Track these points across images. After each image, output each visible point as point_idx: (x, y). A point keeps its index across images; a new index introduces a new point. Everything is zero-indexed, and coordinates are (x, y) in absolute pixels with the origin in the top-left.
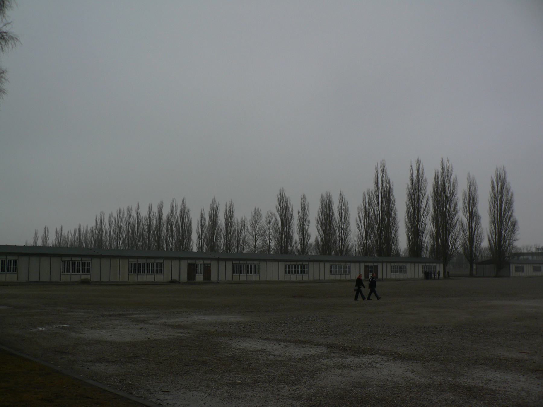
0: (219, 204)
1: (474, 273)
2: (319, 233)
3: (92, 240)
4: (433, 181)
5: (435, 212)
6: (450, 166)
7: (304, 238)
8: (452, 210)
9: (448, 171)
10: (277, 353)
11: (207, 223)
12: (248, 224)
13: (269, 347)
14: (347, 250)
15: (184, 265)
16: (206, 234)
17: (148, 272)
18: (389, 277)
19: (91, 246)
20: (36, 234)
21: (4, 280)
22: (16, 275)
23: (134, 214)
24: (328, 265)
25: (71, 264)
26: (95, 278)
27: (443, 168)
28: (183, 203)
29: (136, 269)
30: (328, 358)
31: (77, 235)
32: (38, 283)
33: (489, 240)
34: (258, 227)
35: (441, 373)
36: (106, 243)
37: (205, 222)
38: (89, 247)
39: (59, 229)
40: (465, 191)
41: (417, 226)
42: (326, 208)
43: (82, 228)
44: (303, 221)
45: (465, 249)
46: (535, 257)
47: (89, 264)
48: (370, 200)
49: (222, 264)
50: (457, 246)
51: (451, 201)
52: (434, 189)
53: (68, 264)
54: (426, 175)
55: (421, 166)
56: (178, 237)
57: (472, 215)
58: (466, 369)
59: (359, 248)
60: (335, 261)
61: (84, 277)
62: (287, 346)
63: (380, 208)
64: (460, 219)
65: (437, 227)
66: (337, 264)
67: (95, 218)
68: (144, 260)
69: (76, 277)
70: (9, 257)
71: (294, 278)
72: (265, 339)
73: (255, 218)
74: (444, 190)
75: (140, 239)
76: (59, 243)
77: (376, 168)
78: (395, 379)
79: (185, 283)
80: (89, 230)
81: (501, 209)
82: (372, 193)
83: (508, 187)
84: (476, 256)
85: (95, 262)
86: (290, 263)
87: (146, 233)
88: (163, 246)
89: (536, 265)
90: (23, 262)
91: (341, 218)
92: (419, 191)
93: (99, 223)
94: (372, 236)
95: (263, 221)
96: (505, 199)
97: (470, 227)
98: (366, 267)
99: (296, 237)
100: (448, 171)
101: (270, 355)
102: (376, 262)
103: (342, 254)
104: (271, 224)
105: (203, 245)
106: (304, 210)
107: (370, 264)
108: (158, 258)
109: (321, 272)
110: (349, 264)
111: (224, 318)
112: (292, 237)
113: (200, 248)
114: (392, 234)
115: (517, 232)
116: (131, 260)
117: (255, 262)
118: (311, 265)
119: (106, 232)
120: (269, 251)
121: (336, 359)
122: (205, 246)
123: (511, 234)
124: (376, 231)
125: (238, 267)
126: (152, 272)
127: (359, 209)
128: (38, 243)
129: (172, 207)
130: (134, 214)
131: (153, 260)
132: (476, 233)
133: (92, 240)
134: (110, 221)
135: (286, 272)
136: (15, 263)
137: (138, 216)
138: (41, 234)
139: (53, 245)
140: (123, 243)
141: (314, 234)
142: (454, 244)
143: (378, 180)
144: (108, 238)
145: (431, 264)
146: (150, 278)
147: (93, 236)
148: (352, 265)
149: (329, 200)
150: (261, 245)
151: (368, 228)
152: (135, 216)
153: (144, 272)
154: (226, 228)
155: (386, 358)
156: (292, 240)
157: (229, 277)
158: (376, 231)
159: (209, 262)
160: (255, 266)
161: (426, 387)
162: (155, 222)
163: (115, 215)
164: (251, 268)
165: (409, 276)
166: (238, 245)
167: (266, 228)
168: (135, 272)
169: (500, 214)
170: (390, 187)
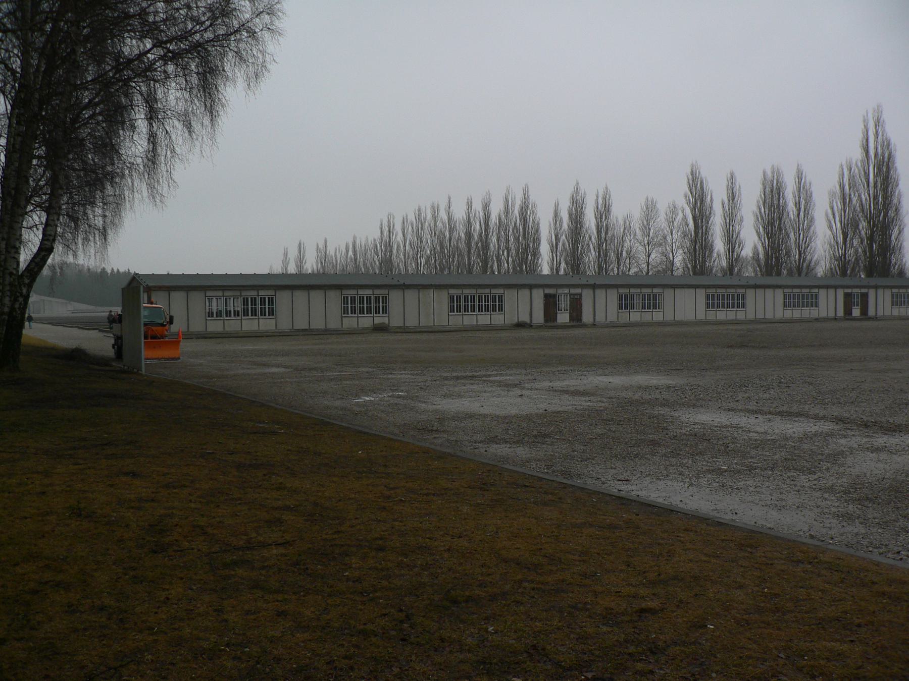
0: (585, 194)
2: (760, 238)
7: (733, 248)
10: (758, 429)
11: (565, 226)
12: (636, 226)
14: (809, 266)
15: (538, 297)
16: (564, 244)
17: (480, 310)
18: (887, 313)
19: (374, 269)
21: (255, 328)
22: (274, 321)
23: (443, 215)
24: (779, 293)
26: (396, 322)
28: (525, 194)
29: (455, 305)
31: (351, 253)
32: (308, 333)
37: (561, 226)
38: (371, 272)
39: (321, 246)
42: (773, 195)
43: (358, 242)
47: (385, 300)
48: (852, 178)
49: (600, 293)
61: (378, 320)
63: (871, 192)
66: (795, 290)
67: (379, 224)
68: (474, 291)
69: (366, 321)
70: (262, 293)
71: (721, 315)
73: (647, 215)
75: (454, 257)
76: (323, 267)
77: (864, 121)
79: (540, 327)
82: (857, 166)
85: (395, 298)
87: (462, 245)
88: (492, 266)
90: (283, 299)
91: (799, 210)
93: (386, 233)
95: (661, 221)
98: (847, 295)
99: (719, 246)
103: (800, 275)
104: (675, 224)
106: (733, 199)
107: (855, 290)
109: (767, 306)
110: (816, 290)
112: (712, 246)
114: (893, 238)
116: (452, 291)
117: (655, 290)
118: (750, 293)
119: (398, 246)
120: (672, 271)
121: (859, 438)
122: (563, 265)
124: (863, 233)
125: (487, 300)
127: (832, 194)
130: (443, 215)
131: (487, 291)
135: (708, 306)
136: (271, 301)
137: (450, 219)
138: (293, 254)
140: (426, 263)
141: (751, 241)
143: (867, 140)
144: (402, 256)
146: (484, 319)
148: (822, 293)
149: (778, 181)
151: (849, 227)
152: (445, 218)
154: (599, 232)
156: (711, 251)
157: (612, 317)
158: (863, 233)
159: (578, 291)
162: (478, 227)
163: (412, 217)
164: (649, 299)
166: (618, 262)
167: (667, 231)
168: (459, 310)
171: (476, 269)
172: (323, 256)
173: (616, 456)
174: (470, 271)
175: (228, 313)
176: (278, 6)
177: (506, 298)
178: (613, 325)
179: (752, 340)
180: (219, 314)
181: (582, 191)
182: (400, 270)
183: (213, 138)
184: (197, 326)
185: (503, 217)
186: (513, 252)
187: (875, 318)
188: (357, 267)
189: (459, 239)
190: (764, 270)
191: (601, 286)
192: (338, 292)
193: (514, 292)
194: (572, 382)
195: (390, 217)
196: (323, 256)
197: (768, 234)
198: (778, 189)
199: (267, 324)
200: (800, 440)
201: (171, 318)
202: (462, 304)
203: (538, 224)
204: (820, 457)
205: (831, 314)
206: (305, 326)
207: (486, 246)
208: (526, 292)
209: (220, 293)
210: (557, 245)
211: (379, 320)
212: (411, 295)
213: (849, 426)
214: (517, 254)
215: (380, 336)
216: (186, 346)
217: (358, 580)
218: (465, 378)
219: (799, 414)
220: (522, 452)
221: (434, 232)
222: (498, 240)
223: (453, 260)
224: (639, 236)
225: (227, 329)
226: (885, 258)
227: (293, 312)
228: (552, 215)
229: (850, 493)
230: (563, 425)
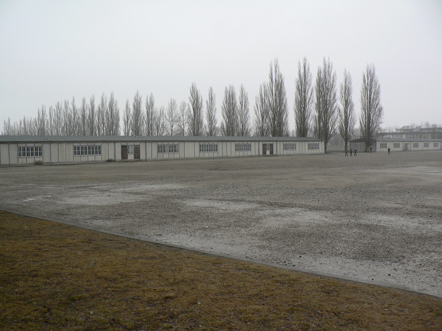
3: (36, 129)
5: (318, 100)
6: (331, 63)
7: (212, 123)
8: (332, 99)
9: (329, 67)
10: (223, 208)
11: (132, 112)
12: (166, 112)
13: (216, 204)
14: (247, 131)
15: (118, 147)
16: (131, 121)
17: (89, 153)
18: (282, 153)
19: (35, 134)
23: (70, 106)
24: (233, 144)
25: (26, 149)
27: (325, 65)
28: (111, 96)
30: (262, 210)
31: (22, 125)
33: (361, 123)
36: (48, 131)
37: (129, 112)
38: (33, 135)
41: (304, 111)
42: (230, 99)
44: (211, 109)
45: (341, 130)
46: (395, 136)
48: (265, 91)
49: (149, 145)
50: (335, 127)
52: (317, 81)
56: (108, 124)
57: (347, 103)
58: (363, 214)
60: (286, 141)
62: (228, 204)
63: (274, 98)
64: (338, 106)
65: (319, 112)
67: (38, 110)
68: (86, 144)
69: (31, 160)
71: (207, 155)
72: (209, 199)
73: (171, 107)
74: (326, 83)
75: (76, 127)
76: (8, 132)
81: (370, 98)
83: (376, 80)
84: (350, 136)
85: (46, 148)
87: (81, 121)
88: (95, 132)
89: (396, 142)
91: (242, 105)
92: (306, 83)
93: (41, 115)
94: (267, 120)
95: (178, 110)
96: (373, 90)
97: (346, 112)
98: (264, 145)
99: (205, 122)
100: (329, 67)
101: (219, 209)
102: (272, 141)
103: (243, 136)
104: (185, 111)
105: (129, 130)
106: (212, 100)
107: (267, 143)
109: (228, 150)
110: (250, 143)
111: (168, 186)
112: (202, 122)
113: (127, 133)
115: (382, 117)
116: (75, 144)
117: (175, 143)
118: (220, 144)
119: (48, 122)
120: (183, 134)
122: (131, 131)
123: (377, 118)
124: (270, 116)
127: (257, 98)
129: (103, 99)
130: (70, 106)
131: (93, 144)
133: (36, 129)
135: (200, 151)
137: (74, 108)
140: (62, 130)
141: (220, 120)
142: (333, 126)
143: (272, 74)
144: (49, 127)
145: (315, 143)
146: (91, 158)
147: (36, 125)
150: (177, 129)
151: (264, 114)
155: (303, 209)
156: (202, 125)
157: (155, 156)
158: (270, 116)
159: (138, 144)
160: (175, 146)
162: (88, 112)
163: (54, 107)
164: (172, 147)
165: (298, 152)
167: (181, 115)
168: (78, 154)
169: (370, 102)
170: (282, 81)
171: (88, 133)
173: (155, 224)
174: (84, 135)
177: (102, 148)
178: (155, 160)
179: (220, 166)
181: (140, 95)
182: (48, 134)
185: (101, 107)
186: (106, 125)
187: (276, 155)
188: (26, 132)
189: (79, 118)
190: (226, 133)
191: (149, 141)
192: (16, 145)
194: (134, 188)
195: (43, 106)
197: (228, 116)
198: (232, 95)
200: (242, 212)
204: (251, 220)
205: (257, 154)
206: (7, 163)
207: (92, 122)
208: (112, 144)
210: (127, 121)
211: (38, 159)
212: (54, 146)
213: (264, 205)
214: (108, 126)
215: (39, 167)
217: (23, 293)
219: (242, 201)
220: (109, 223)
221: (66, 114)
222: (98, 119)
223: (76, 129)
224: (167, 117)
226: (280, 128)
228: (125, 106)
229: (264, 236)
230: (130, 209)
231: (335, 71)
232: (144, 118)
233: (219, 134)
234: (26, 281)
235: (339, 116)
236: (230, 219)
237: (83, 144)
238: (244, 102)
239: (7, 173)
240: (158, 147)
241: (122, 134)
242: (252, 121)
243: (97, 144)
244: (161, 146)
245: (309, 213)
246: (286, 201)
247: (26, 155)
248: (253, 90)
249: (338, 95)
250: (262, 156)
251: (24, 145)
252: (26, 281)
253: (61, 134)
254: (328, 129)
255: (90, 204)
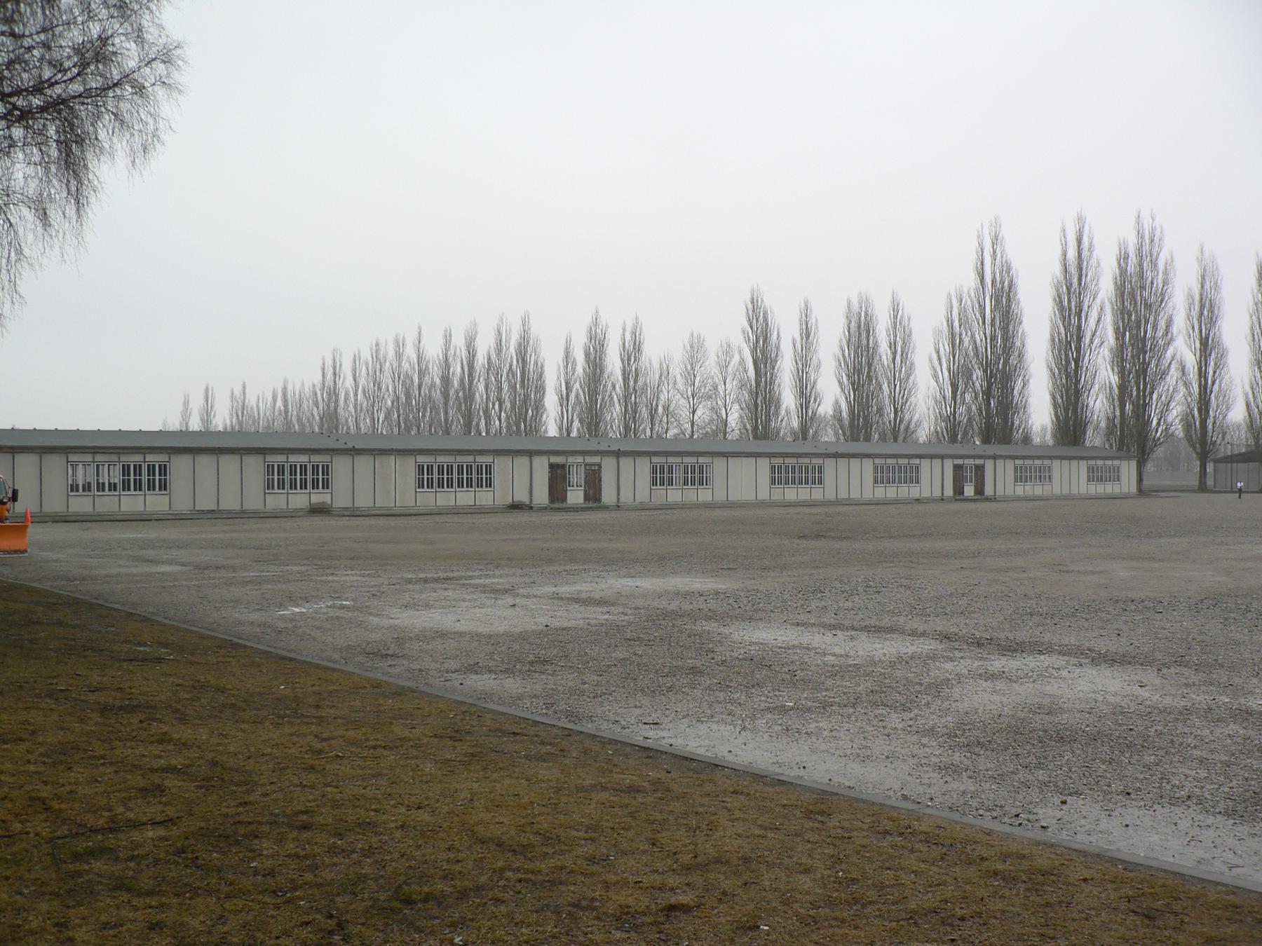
1: (1210, 482)
4: (1115, 264)
5: (1117, 339)
6: (1158, 230)
8: (1160, 333)
10: (837, 650)
11: (580, 370)
12: (676, 371)
13: (817, 639)
15: (541, 467)
16: (577, 396)
17: (460, 485)
18: (1009, 492)
19: (312, 427)
20: (186, 403)
22: (167, 498)
24: (868, 465)
27: (1140, 234)
29: (425, 478)
31: (279, 403)
32: (215, 515)
33: (1248, 405)
34: (698, 378)
35: (1203, 688)
37: (574, 369)
38: (308, 430)
39: (237, 393)
40: (1190, 289)
41: (1076, 371)
43: (290, 388)
44: (804, 363)
45: (1188, 426)
49: (626, 463)
50: (1170, 419)
51: (1157, 314)
53: (281, 470)
54: (1097, 252)
55: (1086, 229)
57: (1207, 346)
59: (936, 424)
60: (1023, 458)
63: (988, 332)
64: (1178, 356)
65: (1122, 373)
68: (450, 459)
69: (299, 500)
71: (791, 494)
73: (692, 357)
74: (1143, 288)
75: (425, 410)
76: (240, 423)
78: (1112, 699)
80: (307, 390)
84: (1214, 443)
85: (340, 466)
86: (781, 460)
87: (437, 395)
88: (478, 425)
90: (180, 468)
91: (894, 353)
93: (329, 376)
94: (968, 397)
95: (710, 366)
97: (1202, 374)
98: (957, 468)
99: (788, 400)
102: (980, 457)
103: (896, 440)
104: (730, 369)
106: (808, 336)
107: (967, 461)
108: (482, 452)
109: (852, 481)
110: (917, 461)
112: (779, 400)
116: (421, 459)
117: (701, 460)
118: (829, 465)
119: (347, 394)
122: (576, 424)
125: (693, 472)
126: (470, 485)
127: (938, 333)
128: (190, 424)
131: (470, 459)
132: (1216, 387)
134: (354, 370)
135: (773, 482)
136: (164, 470)
137: (419, 358)
138: (197, 403)
139: (225, 428)
140: (386, 418)
141: (831, 394)
143: (982, 264)
145: (1109, 463)
146: (465, 497)
149: (866, 314)
150: (707, 419)
151: (959, 378)
153: (450, 485)
155: (1073, 660)
156: (778, 407)
157: (643, 494)
158: (977, 384)
159: (596, 459)
161: (1180, 713)
162: (459, 370)
163: (366, 355)
164: (693, 472)
165: (1057, 491)
167: (718, 379)
168: (430, 485)
171: (456, 428)
172: (240, 408)
175: (101, 487)
176: (178, 52)
177: (496, 469)
178: (643, 508)
179: (830, 528)
180: (87, 487)
181: (602, 322)
182: (348, 428)
183: (79, 235)
184: (54, 504)
185: (494, 357)
186: (508, 405)
187: (993, 499)
188: (288, 423)
189: (433, 385)
190: (848, 433)
192: (260, 458)
193: (507, 460)
194: (584, 587)
195: (336, 353)
196: (240, 408)
197: (853, 384)
198: (867, 325)
199: (155, 502)
200: (892, 665)
201: (15, 492)
202: (435, 476)
203: (542, 366)
207: (469, 397)
208: (524, 460)
209: (89, 458)
211: (319, 497)
212: (363, 463)
213: (956, 645)
214: (513, 407)
215: (319, 521)
216: (35, 533)
217: (271, 873)
218: (436, 580)
219: (891, 630)
220: (512, 685)
221: (397, 375)
222: (487, 388)
223: (424, 416)
224: (680, 385)
225: (99, 509)
226: (1006, 420)
227: (193, 485)
228: (561, 354)
230: (570, 647)
231: (1171, 254)
232: (614, 388)
233: (828, 436)
234: (280, 840)
235: (1180, 383)
236: (858, 685)
237: (442, 459)
238: (900, 343)
239: (234, 535)
240: (654, 471)
241: (552, 431)
242: (925, 397)
243: (484, 460)
244: (662, 467)
245: (1091, 672)
246: (1023, 635)
247: (455, 484)
248: (927, 310)
249: (1180, 323)
250: (951, 500)
251: (281, 458)
252: (280, 840)
253: (382, 429)
254: (1149, 422)
255: (459, 627)
